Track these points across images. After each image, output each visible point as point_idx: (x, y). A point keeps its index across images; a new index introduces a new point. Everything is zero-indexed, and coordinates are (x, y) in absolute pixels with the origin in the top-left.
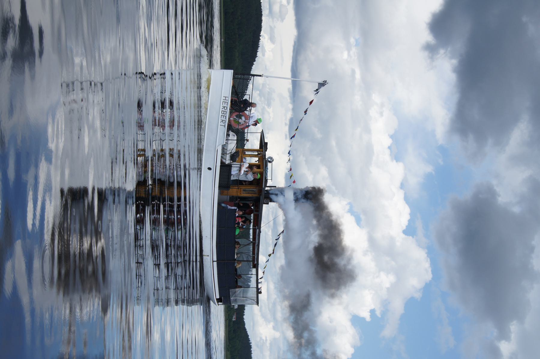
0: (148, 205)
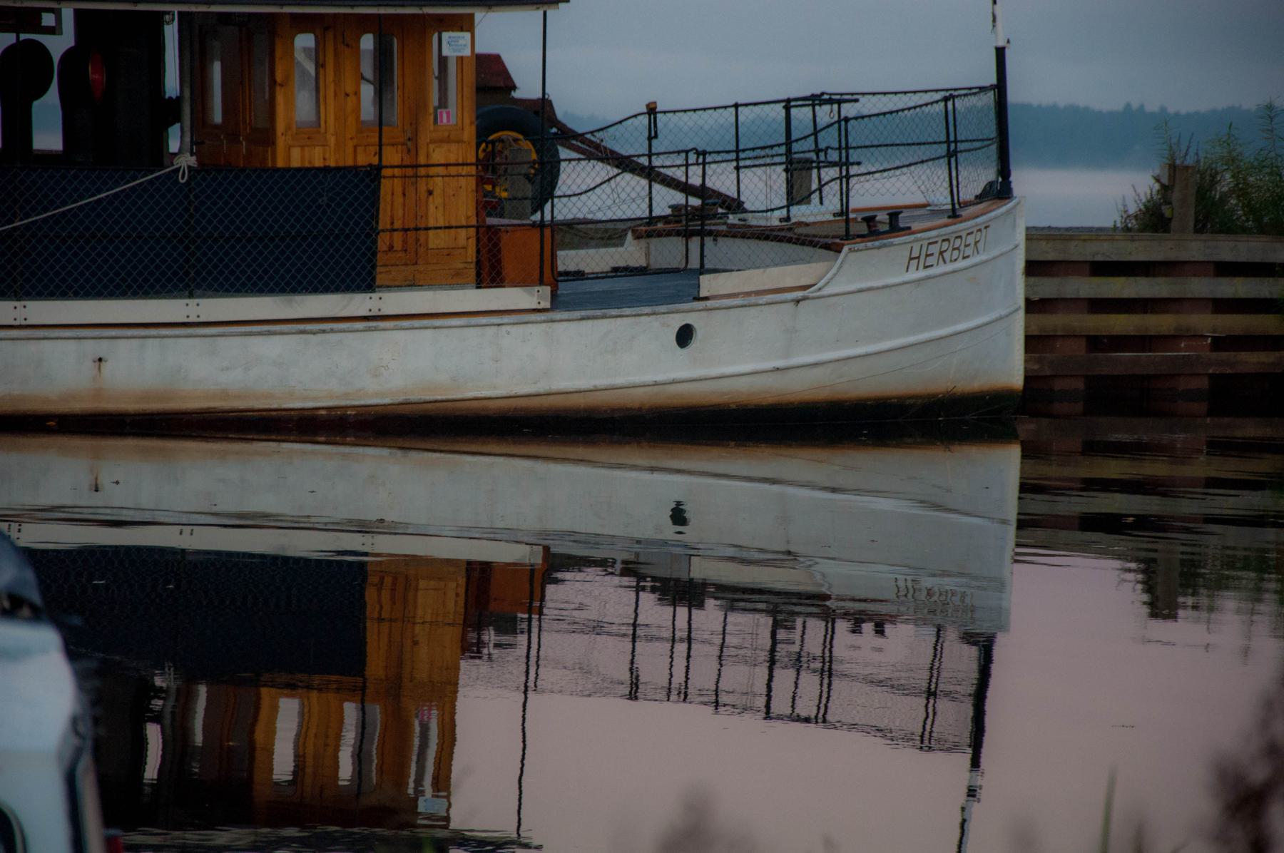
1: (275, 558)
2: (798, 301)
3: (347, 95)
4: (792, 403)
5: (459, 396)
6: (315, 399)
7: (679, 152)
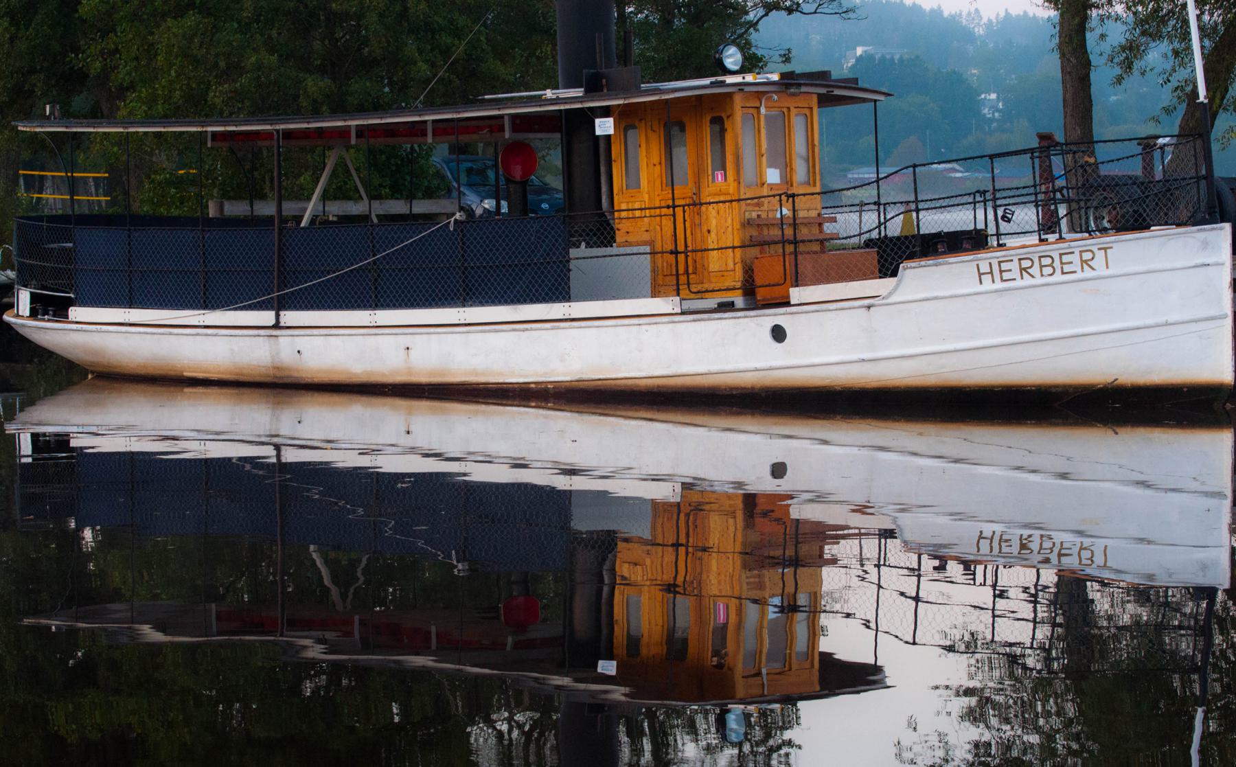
0: (17, 127)
1: (513, 485)
2: (869, 307)
3: (655, 165)
4: (898, 387)
5: (614, 376)
6: (526, 376)
7: (970, 194)
